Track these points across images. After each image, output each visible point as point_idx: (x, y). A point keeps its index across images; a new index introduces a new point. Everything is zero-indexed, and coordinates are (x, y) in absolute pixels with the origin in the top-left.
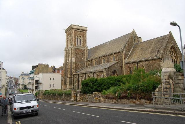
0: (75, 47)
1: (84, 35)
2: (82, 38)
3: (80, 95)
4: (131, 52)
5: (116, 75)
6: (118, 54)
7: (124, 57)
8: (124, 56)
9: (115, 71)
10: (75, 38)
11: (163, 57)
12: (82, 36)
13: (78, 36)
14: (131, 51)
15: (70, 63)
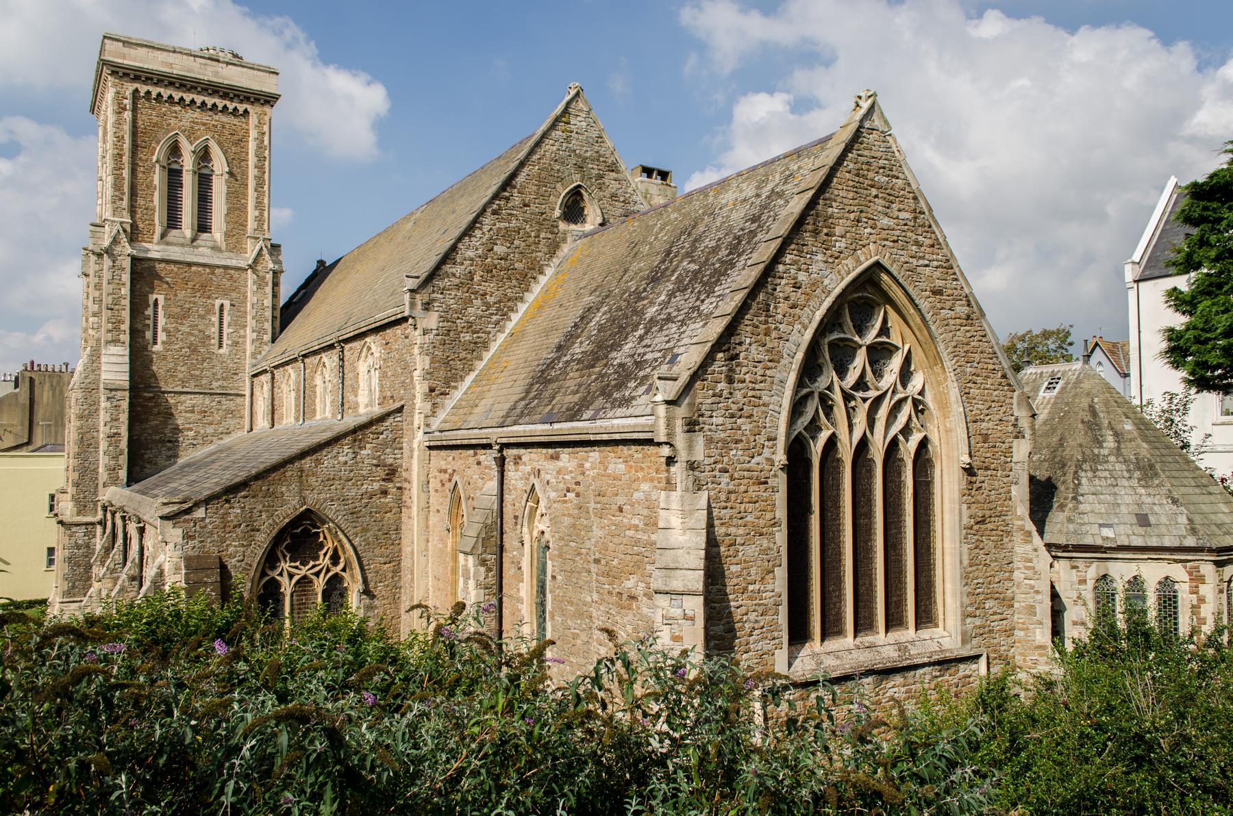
1: (241, 142)
7: (428, 375)
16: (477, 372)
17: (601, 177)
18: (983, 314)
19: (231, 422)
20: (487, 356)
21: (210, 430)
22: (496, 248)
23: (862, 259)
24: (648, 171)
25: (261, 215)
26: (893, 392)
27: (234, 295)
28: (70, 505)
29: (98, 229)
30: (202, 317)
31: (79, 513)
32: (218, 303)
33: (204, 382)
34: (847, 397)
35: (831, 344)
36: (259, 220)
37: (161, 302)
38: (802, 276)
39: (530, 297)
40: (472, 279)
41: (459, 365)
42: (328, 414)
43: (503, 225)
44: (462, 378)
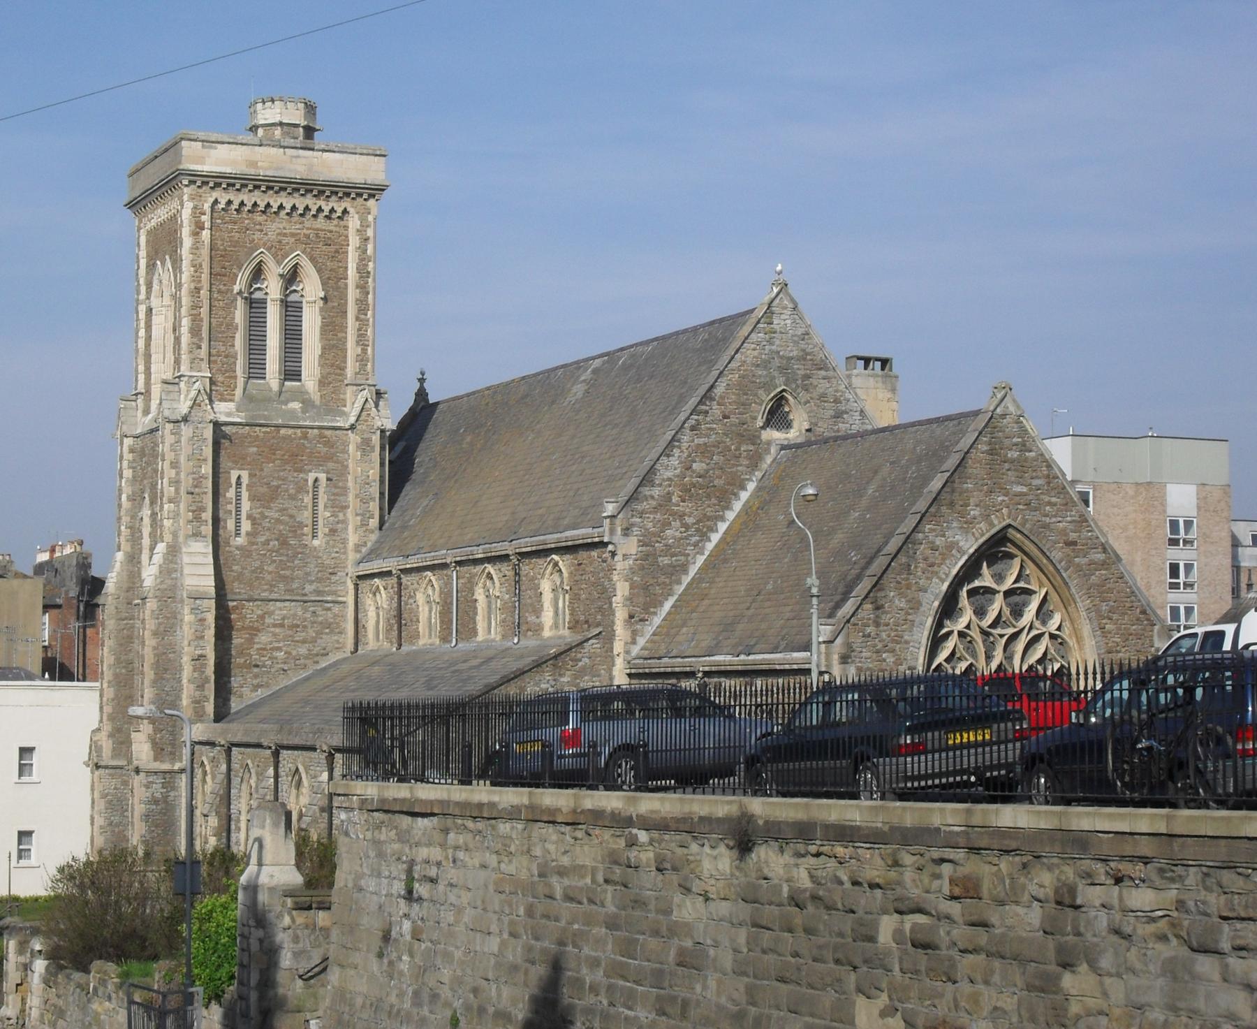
0: (225, 411)
1: (339, 253)
2: (311, 288)
4: (715, 538)
6: (583, 554)
7: (630, 599)
14: (723, 527)
15: (151, 605)
16: (676, 597)
17: (807, 377)
18: (1119, 559)
19: (327, 640)
20: (686, 580)
21: (303, 650)
22: (694, 465)
23: (996, 522)
25: (364, 351)
26: (1031, 628)
27: (331, 465)
29: (170, 387)
30: (292, 498)
31: (156, 759)
32: (311, 477)
33: (295, 586)
34: (985, 633)
35: (971, 593)
36: (362, 360)
38: (939, 541)
39: (731, 515)
40: (670, 500)
41: (658, 590)
42: (496, 635)
43: (701, 441)
44: (661, 604)
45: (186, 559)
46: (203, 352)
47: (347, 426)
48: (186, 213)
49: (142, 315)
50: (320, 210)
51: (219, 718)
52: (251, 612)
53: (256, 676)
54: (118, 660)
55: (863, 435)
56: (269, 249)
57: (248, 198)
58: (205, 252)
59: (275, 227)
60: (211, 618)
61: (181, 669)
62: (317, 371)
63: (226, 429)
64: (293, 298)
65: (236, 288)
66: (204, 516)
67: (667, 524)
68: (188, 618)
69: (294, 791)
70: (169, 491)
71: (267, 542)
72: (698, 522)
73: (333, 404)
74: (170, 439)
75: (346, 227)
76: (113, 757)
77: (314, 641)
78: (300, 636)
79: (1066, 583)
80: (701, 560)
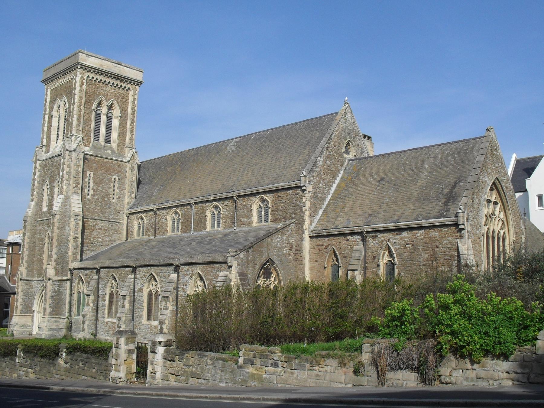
0: (87, 149)
1: (126, 102)
2: (116, 112)
3: (168, 358)
5: (272, 279)
8: (308, 204)
9: (269, 261)
10: (88, 111)
11: (467, 219)
12: (116, 106)
13: (99, 104)
14: (335, 186)
15: (57, 217)
19: (116, 236)
21: (108, 239)
24: (365, 136)
25: (132, 136)
27: (120, 174)
28: (53, 270)
30: (107, 184)
32: (114, 177)
36: (131, 139)
37: (92, 176)
45: (72, 201)
46: (81, 128)
47: (127, 161)
48: (78, 79)
49: (47, 118)
50: (121, 86)
51: (81, 260)
52: (91, 223)
53: (92, 247)
54: (30, 241)
55: (367, 158)
56: (104, 96)
57: (99, 77)
58: (84, 93)
59: (107, 89)
60: (80, 223)
61: (68, 241)
62: (117, 141)
63: (87, 156)
64: (110, 115)
65: (93, 108)
66: (79, 186)
67: (320, 182)
68: (73, 222)
69: (147, 283)
70: (66, 176)
71: (98, 199)
72: (328, 183)
73: (121, 153)
74: (67, 157)
75: (129, 94)
76: (27, 276)
77: (111, 236)
78: (107, 234)
79: (507, 201)
80: (329, 197)
